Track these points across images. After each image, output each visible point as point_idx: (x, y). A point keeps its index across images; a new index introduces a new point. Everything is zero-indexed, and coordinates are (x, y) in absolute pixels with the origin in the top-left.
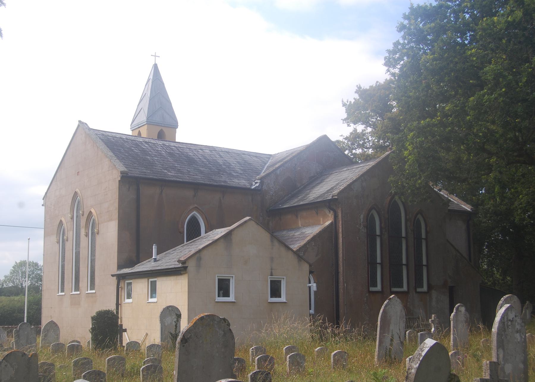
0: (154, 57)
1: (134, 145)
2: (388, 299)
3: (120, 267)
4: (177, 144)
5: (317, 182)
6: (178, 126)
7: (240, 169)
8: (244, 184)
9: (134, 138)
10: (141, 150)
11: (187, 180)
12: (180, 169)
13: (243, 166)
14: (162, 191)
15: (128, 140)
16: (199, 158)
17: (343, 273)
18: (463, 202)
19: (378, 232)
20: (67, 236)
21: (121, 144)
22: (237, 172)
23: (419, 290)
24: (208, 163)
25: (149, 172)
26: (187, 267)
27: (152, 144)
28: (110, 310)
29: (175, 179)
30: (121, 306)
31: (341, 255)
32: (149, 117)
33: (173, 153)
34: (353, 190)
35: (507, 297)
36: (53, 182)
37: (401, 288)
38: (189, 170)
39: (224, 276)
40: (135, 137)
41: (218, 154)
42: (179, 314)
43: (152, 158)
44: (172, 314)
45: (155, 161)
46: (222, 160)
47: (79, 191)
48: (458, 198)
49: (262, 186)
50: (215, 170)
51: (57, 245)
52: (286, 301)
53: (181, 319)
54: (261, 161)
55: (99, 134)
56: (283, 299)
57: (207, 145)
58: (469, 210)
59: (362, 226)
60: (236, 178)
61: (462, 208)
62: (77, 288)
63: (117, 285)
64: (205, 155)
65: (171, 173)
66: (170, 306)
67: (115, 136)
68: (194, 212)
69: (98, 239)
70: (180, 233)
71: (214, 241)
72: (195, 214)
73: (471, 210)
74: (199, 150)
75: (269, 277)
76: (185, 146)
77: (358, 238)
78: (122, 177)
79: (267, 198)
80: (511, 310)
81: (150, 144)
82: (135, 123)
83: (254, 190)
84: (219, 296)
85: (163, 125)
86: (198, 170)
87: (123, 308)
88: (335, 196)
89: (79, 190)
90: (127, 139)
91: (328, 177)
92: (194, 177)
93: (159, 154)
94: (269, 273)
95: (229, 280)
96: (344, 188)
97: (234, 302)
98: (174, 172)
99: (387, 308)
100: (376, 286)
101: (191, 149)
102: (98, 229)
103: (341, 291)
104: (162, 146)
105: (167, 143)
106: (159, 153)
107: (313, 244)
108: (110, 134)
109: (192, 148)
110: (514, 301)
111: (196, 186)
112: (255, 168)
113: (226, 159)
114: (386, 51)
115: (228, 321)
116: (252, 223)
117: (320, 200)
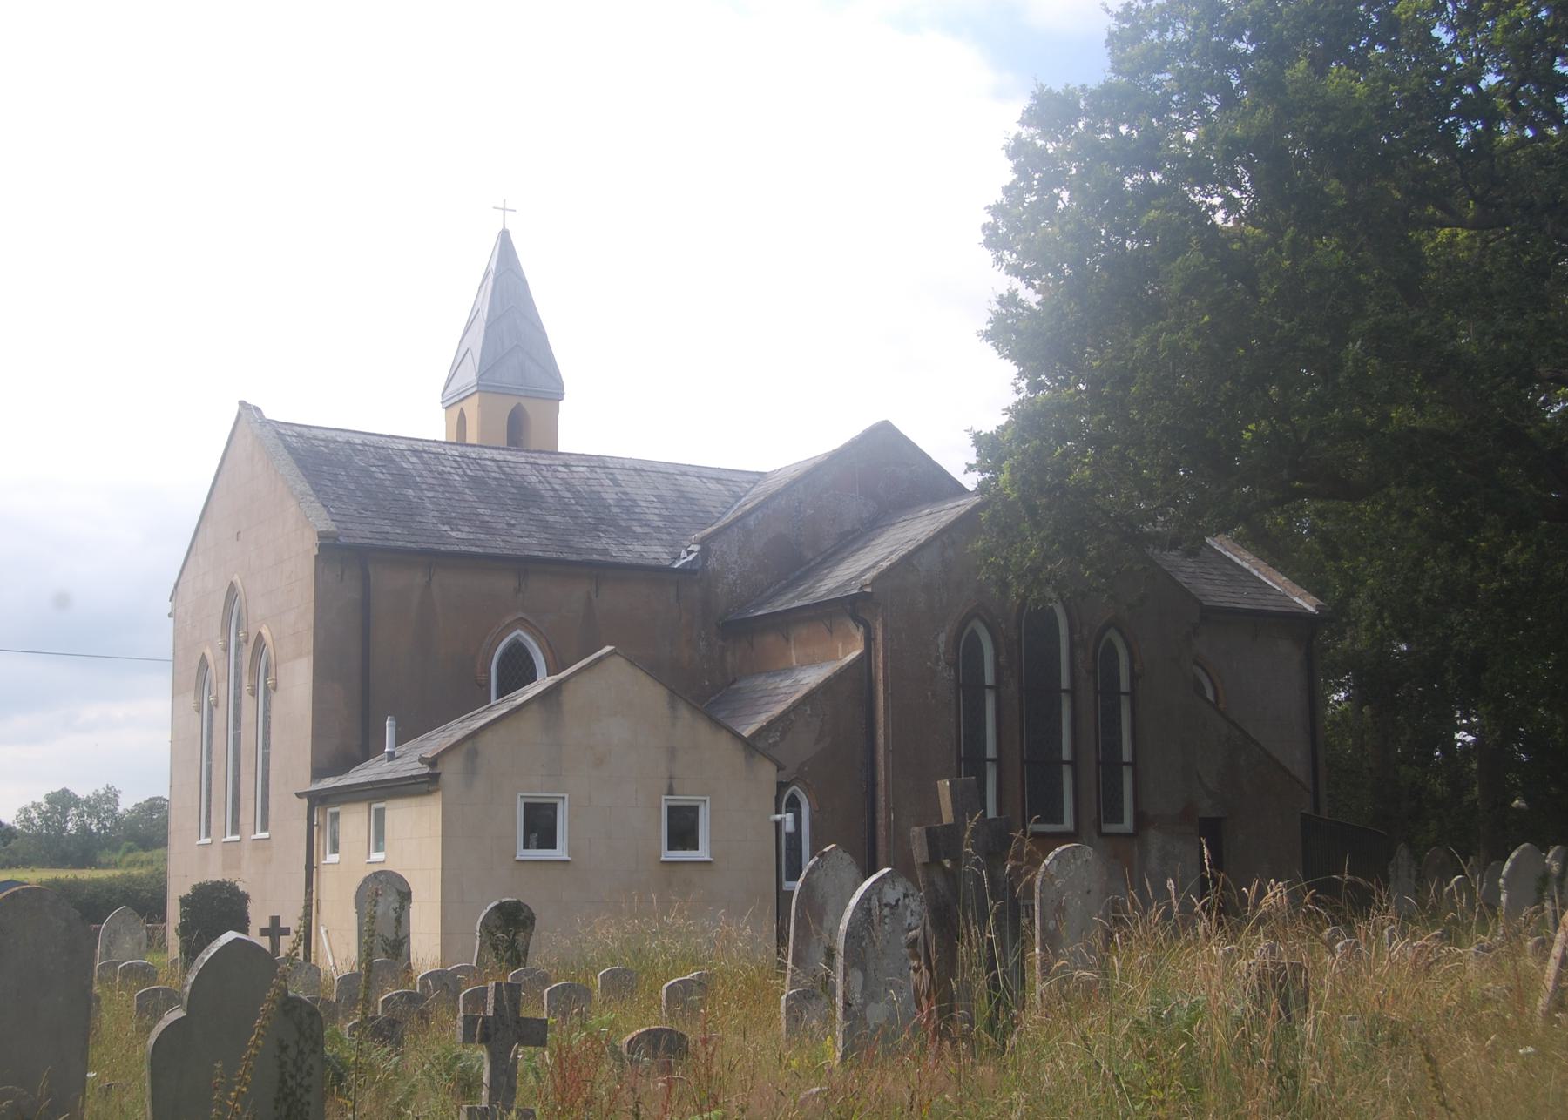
0: (502, 211)
1: (380, 460)
2: (819, 853)
3: (317, 774)
4: (500, 454)
5: (855, 547)
6: (559, 395)
7: (659, 515)
8: (656, 556)
9: (386, 441)
10: (395, 472)
11: (497, 551)
12: (488, 522)
13: (670, 506)
14: (430, 579)
15: (366, 448)
16: (555, 491)
17: (886, 786)
18: (1298, 590)
19: (989, 679)
20: (215, 694)
21: (344, 460)
22: (649, 523)
23: (1109, 828)
24: (573, 501)
25: (398, 531)
26: (440, 774)
27: (432, 456)
28: (227, 880)
29: (466, 549)
30: (318, 872)
31: (881, 740)
32: (483, 374)
33: (484, 478)
34: (918, 570)
35: (1064, 850)
36: (190, 556)
37: (1056, 823)
38: (513, 522)
39: (541, 795)
40: (388, 439)
41: (610, 476)
42: (406, 890)
43: (420, 494)
44: (388, 890)
45: (427, 500)
46: (617, 494)
47: (239, 582)
48: (1286, 576)
49: (705, 560)
50: (589, 520)
51: (197, 716)
52: (712, 859)
53: (411, 902)
54: (729, 490)
55: (289, 435)
56: (702, 853)
57: (585, 453)
58: (1312, 610)
59: (942, 663)
60: (638, 540)
61: (1293, 604)
62: (236, 829)
63: (308, 819)
64: (573, 480)
65: (459, 533)
66: (380, 871)
67: (332, 437)
68: (519, 632)
69: (276, 698)
70: (480, 685)
71: (512, 710)
72: (518, 635)
73: (1317, 610)
74: (560, 468)
75: (664, 797)
76: (522, 456)
77: (929, 694)
78: (321, 547)
79: (719, 590)
80: (893, 882)
81: (425, 455)
82: (451, 388)
83: (685, 571)
84: (526, 846)
85: (522, 393)
86: (541, 521)
87: (322, 875)
88: (866, 585)
89: (240, 578)
90: (364, 444)
91: (883, 532)
92: (521, 540)
93: (442, 482)
94: (665, 789)
95: (554, 806)
96: (891, 565)
97: (567, 861)
98: (467, 529)
99: (815, 876)
100: (1120, 820)
101: (537, 464)
102: (274, 677)
103: (881, 832)
104: (459, 459)
105: (474, 452)
106: (442, 479)
107: (809, 712)
108: (319, 434)
109: (540, 461)
110: (1085, 859)
111: (522, 566)
112: (703, 512)
113: (628, 490)
114: (985, 209)
115: (529, 909)
116: (619, 663)
117: (833, 597)
